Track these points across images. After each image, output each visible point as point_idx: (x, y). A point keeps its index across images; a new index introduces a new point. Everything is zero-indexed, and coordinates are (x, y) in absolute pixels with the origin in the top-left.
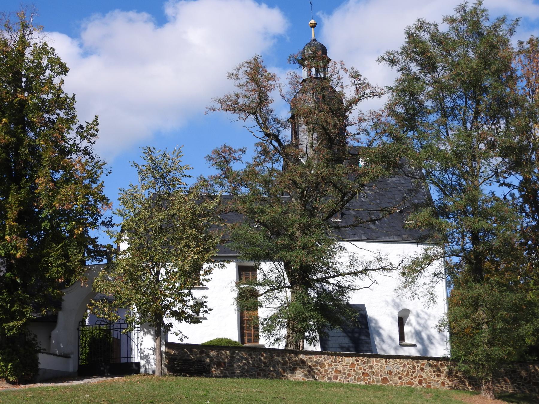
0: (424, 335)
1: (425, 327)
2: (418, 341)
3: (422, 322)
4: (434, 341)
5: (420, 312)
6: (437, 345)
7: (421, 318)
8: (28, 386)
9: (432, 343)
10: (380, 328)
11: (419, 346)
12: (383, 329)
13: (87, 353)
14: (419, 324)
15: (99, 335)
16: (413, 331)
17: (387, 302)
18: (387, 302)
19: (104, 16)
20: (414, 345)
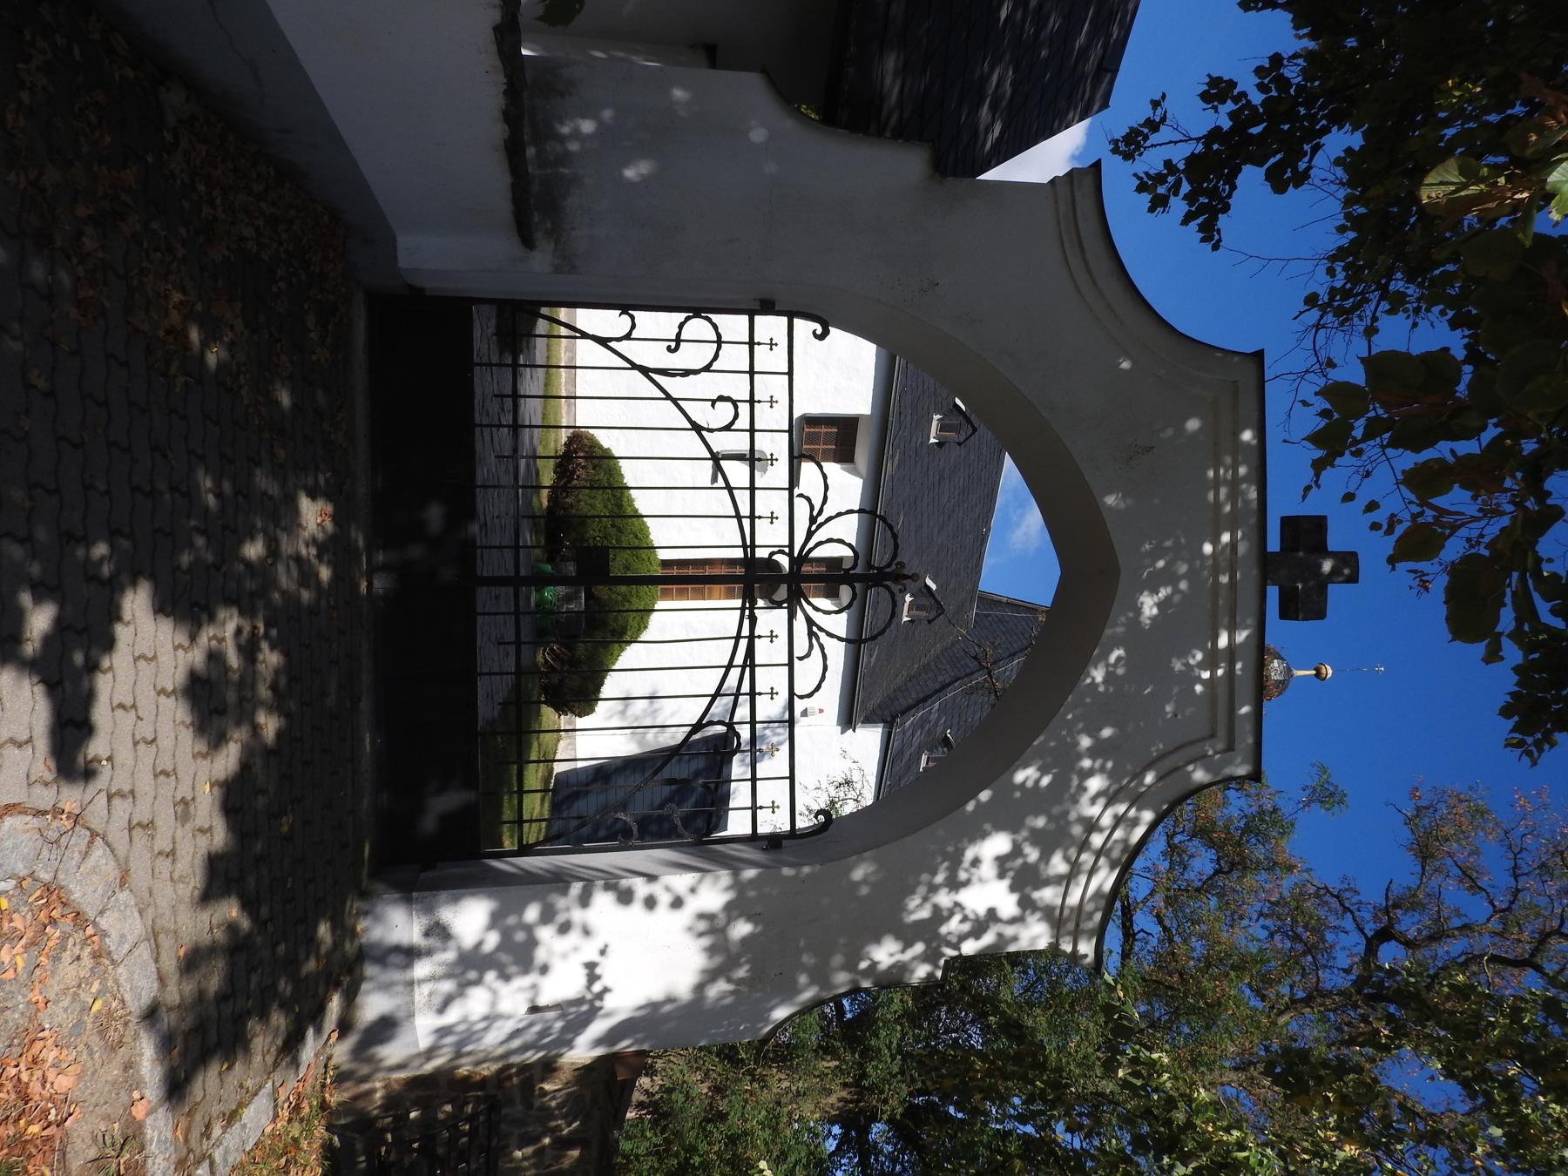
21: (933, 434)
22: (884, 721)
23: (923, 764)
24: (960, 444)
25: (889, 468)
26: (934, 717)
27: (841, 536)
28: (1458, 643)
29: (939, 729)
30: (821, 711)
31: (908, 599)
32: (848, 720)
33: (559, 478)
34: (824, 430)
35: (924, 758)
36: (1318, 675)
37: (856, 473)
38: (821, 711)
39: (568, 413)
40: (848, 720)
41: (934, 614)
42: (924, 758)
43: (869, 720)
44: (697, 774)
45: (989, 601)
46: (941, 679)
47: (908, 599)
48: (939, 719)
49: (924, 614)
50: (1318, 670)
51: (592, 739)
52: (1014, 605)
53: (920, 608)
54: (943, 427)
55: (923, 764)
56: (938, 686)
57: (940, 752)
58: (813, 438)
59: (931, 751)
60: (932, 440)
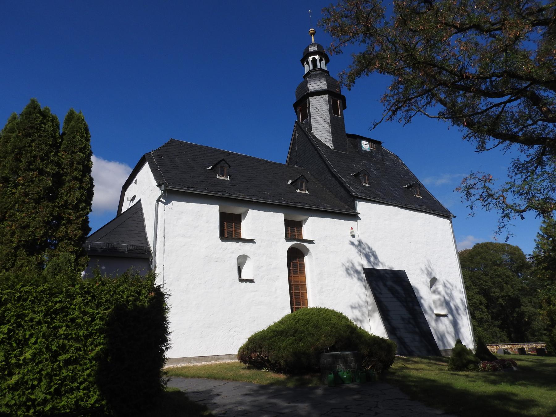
0: (452, 305)
1: (451, 296)
2: (449, 312)
3: (449, 291)
4: (460, 312)
5: (446, 282)
6: (462, 315)
7: (448, 288)
8: (332, 90)
9: (459, 314)
10: (421, 298)
11: (450, 317)
12: (424, 300)
13: (97, 358)
14: (447, 294)
15: (137, 299)
16: (442, 299)
17: (422, 270)
18: (422, 270)
19: (168, 309)
20: (445, 316)
21: (225, 179)
22: (354, 201)
23: (367, 185)
24: (230, 167)
25: (244, 197)
26: (348, 180)
27: (276, 220)
28: (177, 206)
29: (352, 178)
30: (352, 229)
31: (298, 191)
32: (354, 216)
33: (265, 367)
34: (226, 229)
35: (365, 184)
36: (313, 34)
37: (246, 213)
38: (352, 229)
39: (223, 359)
40: (354, 216)
41: (304, 180)
42: (365, 184)
43: (354, 207)
44: (385, 285)
45: (291, 160)
46: (330, 178)
47: (298, 191)
48: (348, 178)
49: (304, 184)
50: (312, 34)
51: (102, 346)
52: (292, 151)
53: (302, 186)
54: (222, 174)
55: (367, 185)
56: (333, 179)
57: (361, 177)
58: (230, 233)
59: (361, 182)
60: (228, 179)
